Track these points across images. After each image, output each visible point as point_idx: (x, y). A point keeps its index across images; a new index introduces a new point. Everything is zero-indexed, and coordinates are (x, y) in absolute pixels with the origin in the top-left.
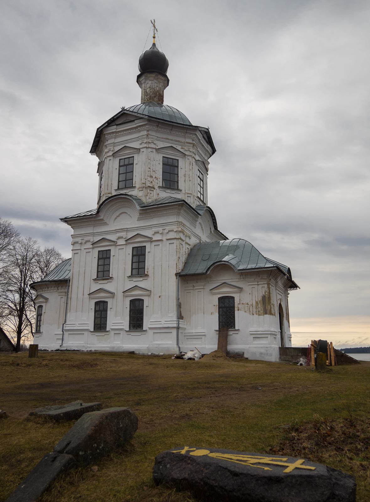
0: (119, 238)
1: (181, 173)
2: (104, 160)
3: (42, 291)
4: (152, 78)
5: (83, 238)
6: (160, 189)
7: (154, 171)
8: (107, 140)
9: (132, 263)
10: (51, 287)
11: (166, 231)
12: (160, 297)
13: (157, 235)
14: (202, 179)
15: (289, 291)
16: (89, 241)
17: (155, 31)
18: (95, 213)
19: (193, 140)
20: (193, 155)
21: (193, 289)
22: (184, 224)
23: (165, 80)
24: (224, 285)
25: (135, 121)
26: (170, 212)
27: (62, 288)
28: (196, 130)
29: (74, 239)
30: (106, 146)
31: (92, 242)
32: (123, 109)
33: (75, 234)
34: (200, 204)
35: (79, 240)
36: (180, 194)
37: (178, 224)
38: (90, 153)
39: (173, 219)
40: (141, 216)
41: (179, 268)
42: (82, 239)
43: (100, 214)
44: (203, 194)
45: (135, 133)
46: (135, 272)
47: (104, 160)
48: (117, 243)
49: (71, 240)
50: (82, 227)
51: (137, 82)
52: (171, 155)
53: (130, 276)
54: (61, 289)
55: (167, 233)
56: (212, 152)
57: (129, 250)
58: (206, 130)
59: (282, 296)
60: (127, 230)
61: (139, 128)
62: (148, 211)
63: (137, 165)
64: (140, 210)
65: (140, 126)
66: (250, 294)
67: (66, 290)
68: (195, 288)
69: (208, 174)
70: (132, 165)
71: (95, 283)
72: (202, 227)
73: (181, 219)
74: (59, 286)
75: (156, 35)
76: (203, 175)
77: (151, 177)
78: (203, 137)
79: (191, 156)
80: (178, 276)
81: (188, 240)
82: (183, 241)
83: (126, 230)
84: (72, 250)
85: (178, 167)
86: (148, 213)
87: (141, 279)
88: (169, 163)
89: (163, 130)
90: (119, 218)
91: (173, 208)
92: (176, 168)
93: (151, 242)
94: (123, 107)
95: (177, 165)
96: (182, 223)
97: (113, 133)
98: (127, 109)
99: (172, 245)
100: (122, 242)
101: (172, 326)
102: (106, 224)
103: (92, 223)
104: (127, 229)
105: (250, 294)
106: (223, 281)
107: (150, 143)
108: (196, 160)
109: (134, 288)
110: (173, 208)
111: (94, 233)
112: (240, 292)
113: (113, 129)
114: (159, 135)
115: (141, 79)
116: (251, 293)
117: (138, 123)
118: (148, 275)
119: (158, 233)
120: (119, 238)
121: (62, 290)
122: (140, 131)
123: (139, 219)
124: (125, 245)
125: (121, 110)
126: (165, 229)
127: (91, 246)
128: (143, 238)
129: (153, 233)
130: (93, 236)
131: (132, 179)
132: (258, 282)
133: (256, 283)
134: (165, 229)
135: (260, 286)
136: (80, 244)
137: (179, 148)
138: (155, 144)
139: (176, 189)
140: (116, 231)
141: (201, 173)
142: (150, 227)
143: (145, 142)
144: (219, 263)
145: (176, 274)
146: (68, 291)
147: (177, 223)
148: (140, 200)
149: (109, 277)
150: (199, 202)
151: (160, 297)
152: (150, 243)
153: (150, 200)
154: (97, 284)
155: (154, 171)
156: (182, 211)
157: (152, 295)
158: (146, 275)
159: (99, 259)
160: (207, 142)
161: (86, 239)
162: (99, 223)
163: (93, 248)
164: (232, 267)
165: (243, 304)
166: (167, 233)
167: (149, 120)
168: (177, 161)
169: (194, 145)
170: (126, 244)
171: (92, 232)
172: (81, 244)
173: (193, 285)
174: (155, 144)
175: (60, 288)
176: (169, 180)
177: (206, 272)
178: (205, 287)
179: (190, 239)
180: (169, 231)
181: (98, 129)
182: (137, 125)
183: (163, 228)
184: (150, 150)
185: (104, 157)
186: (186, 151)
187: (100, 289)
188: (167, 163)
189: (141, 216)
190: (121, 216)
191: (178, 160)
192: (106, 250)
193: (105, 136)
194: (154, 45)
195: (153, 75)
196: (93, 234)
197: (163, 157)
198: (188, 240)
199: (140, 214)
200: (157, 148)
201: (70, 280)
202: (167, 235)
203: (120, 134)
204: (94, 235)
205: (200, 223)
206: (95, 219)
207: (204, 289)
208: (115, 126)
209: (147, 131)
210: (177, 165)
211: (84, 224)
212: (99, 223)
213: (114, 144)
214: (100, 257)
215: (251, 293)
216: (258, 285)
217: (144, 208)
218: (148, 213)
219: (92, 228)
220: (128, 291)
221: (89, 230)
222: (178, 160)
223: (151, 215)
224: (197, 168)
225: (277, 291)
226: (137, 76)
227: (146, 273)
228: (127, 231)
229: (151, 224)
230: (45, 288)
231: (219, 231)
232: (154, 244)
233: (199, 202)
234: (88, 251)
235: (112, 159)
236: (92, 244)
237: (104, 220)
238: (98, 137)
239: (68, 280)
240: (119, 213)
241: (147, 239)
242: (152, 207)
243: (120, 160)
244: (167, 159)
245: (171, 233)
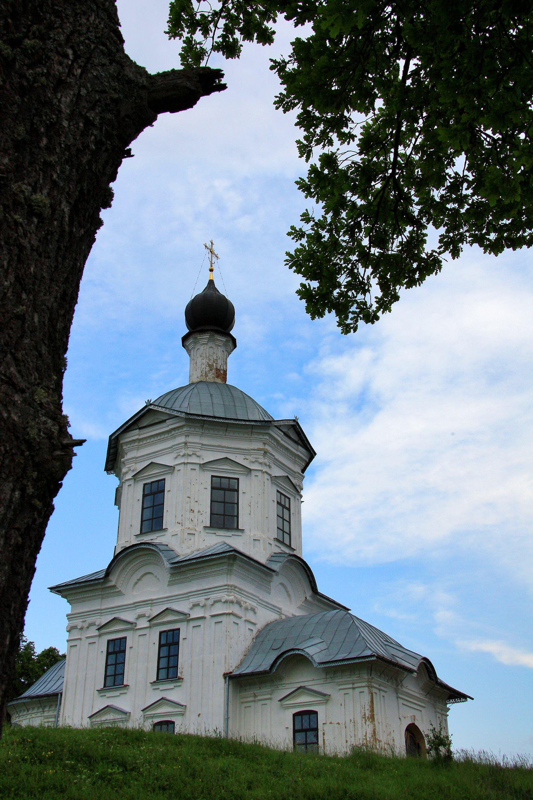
0: (140, 616)
1: (243, 501)
3: (19, 716)
4: (205, 341)
5: (84, 620)
6: (207, 531)
7: (197, 502)
8: (126, 454)
9: (159, 658)
10: (33, 708)
11: (210, 602)
12: (199, 715)
13: (196, 609)
14: (287, 506)
15: (448, 706)
16: (92, 624)
17: (214, 259)
18: (101, 577)
19: (265, 444)
21: (254, 701)
22: (240, 589)
24: (301, 690)
25: (167, 421)
27: (50, 709)
28: (268, 427)
29: (71, 622)
30: (124, 463)
31: (98, 625)
33: (75, 612)
34: (282, 550)
35: (78, 622)
36: (241, 537)
37: (228, 589)
39: (221, 581)
40: (174, 579)
41: (230, 665)
42: (83, 622)
43: (111, 578)
45: (167, 439)
46: (163, 673)
48: (136, 626)
49: (66, 623)
50: (84, 601)
51: (183, 346)
52: (225, 471)
53: (154, 682)
54: (49, 711)
55: (212, 605)
56: (309, 457)
57: (154, 637)
58: (293, 423)
59: (421, 711)
60: (151, 603)
61: (173, 433)
62: (183, 569)
63: (169, 492)
64: (171, 568)
65: (174, 429)
66: (341, 705)
67: (56, 713)
68: (257, 699)
69: (301, 496)
70: (163, 493)
71: (101, 696)
72: (287, 592)
73: (234, 581)
74: (45, 707)
75: (214, 267)
76: (289, 499)
77: (192, 511)
79: (262, 471)
80: (227, 678)
81: (250, 616)
82: (240, 618)
83: (150, 602)
84: (68, 641)
85: (237, 491)
86: (183, 572)
87: (171, 686)
88: (223, 486)
89: (211, 432)
90: (140, 583)
91: (83, 592)
92: (236, 493)
93: (189, 621)
95: (236, 488)
96: (235, 587)
97: (134, 441)
98: (156, 403)
99: (220, 624)
100: (143, 623)
102: (120, 594)
103: (100, 593)
104: (152, 600)
105: (341, 705)
106: (298, 685)
107: (190, 455)
109: (160, 702)
110: (83, 592)
111: (102, 610)
112: (326, 703)
113: (134, 435)
114: (206, 441)
115: (187, 343)
116: (343, 704)
117: (170, 425)
118: (183, 679)
119: (220, 601)
120: (140, 616)
121: (51, 713)
122: (175, 437)
123: (171, 583)
124: (149, 629)
127: (97, 633)
128: (176, 616)
129: (191, 605)
130: (101, 617)
132: (353, 684)
133: (351, 686)
135: (357, 691)
136: (80, 629)
137: (239, 459)
138: (198, 456)
139: (235, 529)
140: (136, 605)
141: (285, 496)
142: (186, 596)
143: (182, 454)
144: (289, 654)
145: (225, 675)
146: (58, 714)
147: (226, 587)
148: (173, 551)
149: (123, 684)
150: (280, 548)
151: (199, 715)
152: (186, 623)
153: (188, 551)
154: (105, 697)
155: (197, 502)
156: (235, 568)
157: (187, 713)
158: (180, 678)
159: (108, 654)
160: (296, 442)
161: (90, 620)
162: (109, 592)
163: (100, 636)
164: (310, 658)
165: (331, 723)
166: (212, 605)
167: (186, 420)
168: (236, 481)
169: (266, 453)
170: (150, 627)
171: (99, 608)
172: (82, 629)
173: (254, 694)
174: (198, 456)
175: (47, 709)
177: (271, 668)
178: (272, 696)
179: (255, 613)
180: (215, 602)
181: (111, 437)
182: (171, 427)
183: (206, 597)
184: (190, 467)
186: (253, 462)
187: (108, 706)
189: (174, 579)
190: (144, 578)
191: (238, 479)
192: (120, 639)
193: (122, 447)
194: (211, 282)
195: (207, 336)
196: (101, 612)
197: (212, 476)
198: (250, 616)
199: (172, 574)
200: (202, 462)
201: (61, 695)
202: (213, 608)
203: (145, 442)
204: (101, 613)
206: (103, 586)
207: (270, 699)
208: (138, 431)
209: (186, 436)
210: (236, 488)
211: (87, 595)
212: (109, 592)
213: (136, 459)
214: (111, 650)
215: (343, 704)
216: (354, 688)
217: (176, 565)
218: (183, 572)
219: (99, 601)
220: (149, 709)
221: (95, 605)
222: (238, 479)
223: (188, 575)
225: (401, 701)
227: (179, 675)
228: (152, 604)
229: (189, 590)
230: (24, 710)
232: (192, 624)
233: (280, 548)
234: (92, 640)
235: (132, 485)
236: (98, 629)
238: (113, 448)
239: (59, 694)
240: (141, 575)
241: (182, 617)
242: (188, 563)
243: (145, 485)
244: (219, 479)
245: (218, 605)
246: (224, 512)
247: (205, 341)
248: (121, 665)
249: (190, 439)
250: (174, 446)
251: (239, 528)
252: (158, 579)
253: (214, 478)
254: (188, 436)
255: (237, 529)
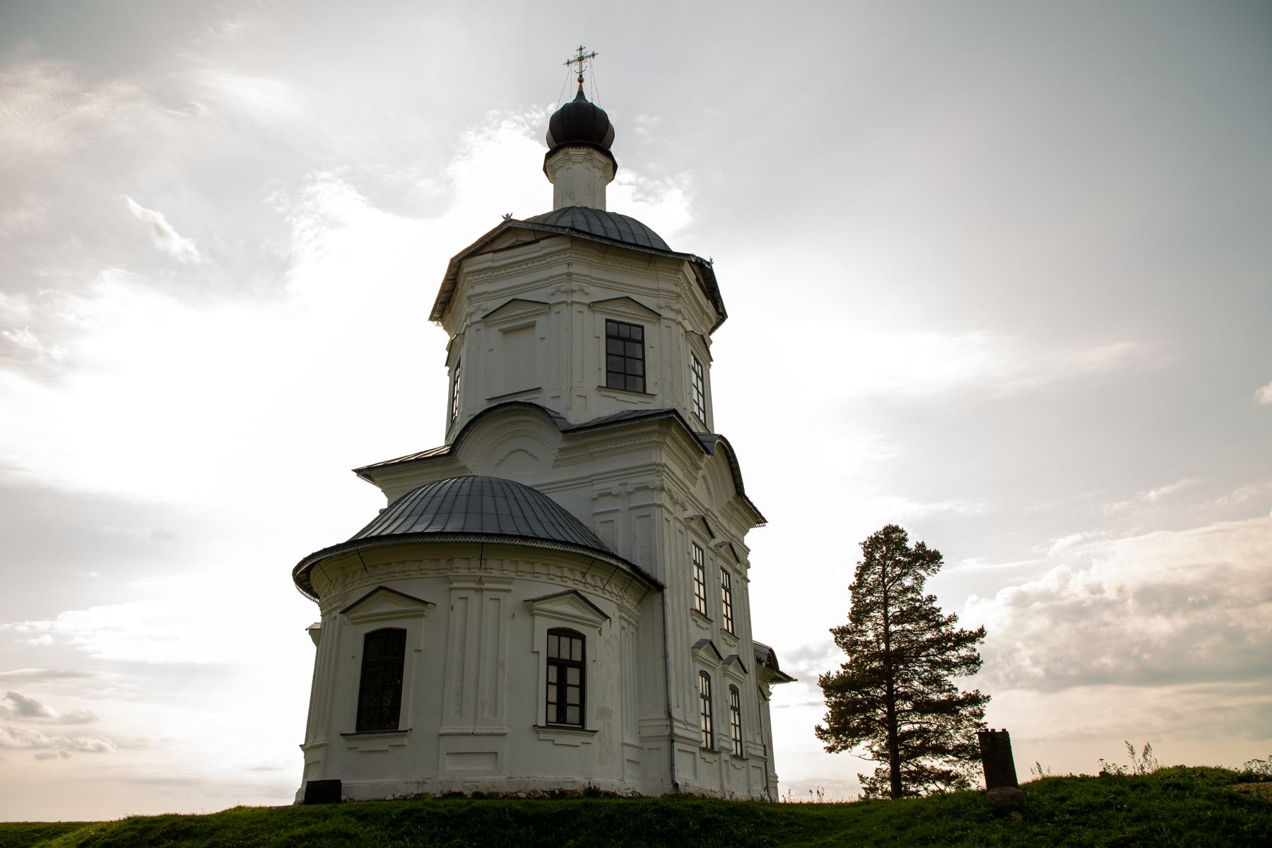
2: (464, 332)
4: (580, 159)
18: (446, 452)
20: (680, 318)
23: (606, 165)
26: (628, 443)
32: (508, 219)
38: (432, 318)
44: (705, 422)
47: (464, 332)
52: (627, 315)
78: (697, 279)
79: (675, 320)
85: (642, 342)
88: (621, 335)
94: (507, 215)
95: (640, 338)
101: (460, 731)
107: (575, 291)
108: (686, 332)
123: (557, 464)
125: (504, 220)
126: (627, 483)
131: (626, 388)
134: (627, 483)
176: (623, 354)
182: (545, 251)
185: (465, 325)
188: (617, 335)
191: (642, 327)
194: (581, 94)
197: (607, 321)
205: (704, 477)
210: (640, 338)
224: (690, 348)
226: (546, 154)
231: (747, 499)
237: (469, 467)
246: (625, 378)
247: (580, 159)
248: (623, 386)
249: (576, 269)
250: (552, 277)
251: (647, 392)
252: (537, 458)
253: (608, 323)
254: (571, 264)
255: (644, 392)
